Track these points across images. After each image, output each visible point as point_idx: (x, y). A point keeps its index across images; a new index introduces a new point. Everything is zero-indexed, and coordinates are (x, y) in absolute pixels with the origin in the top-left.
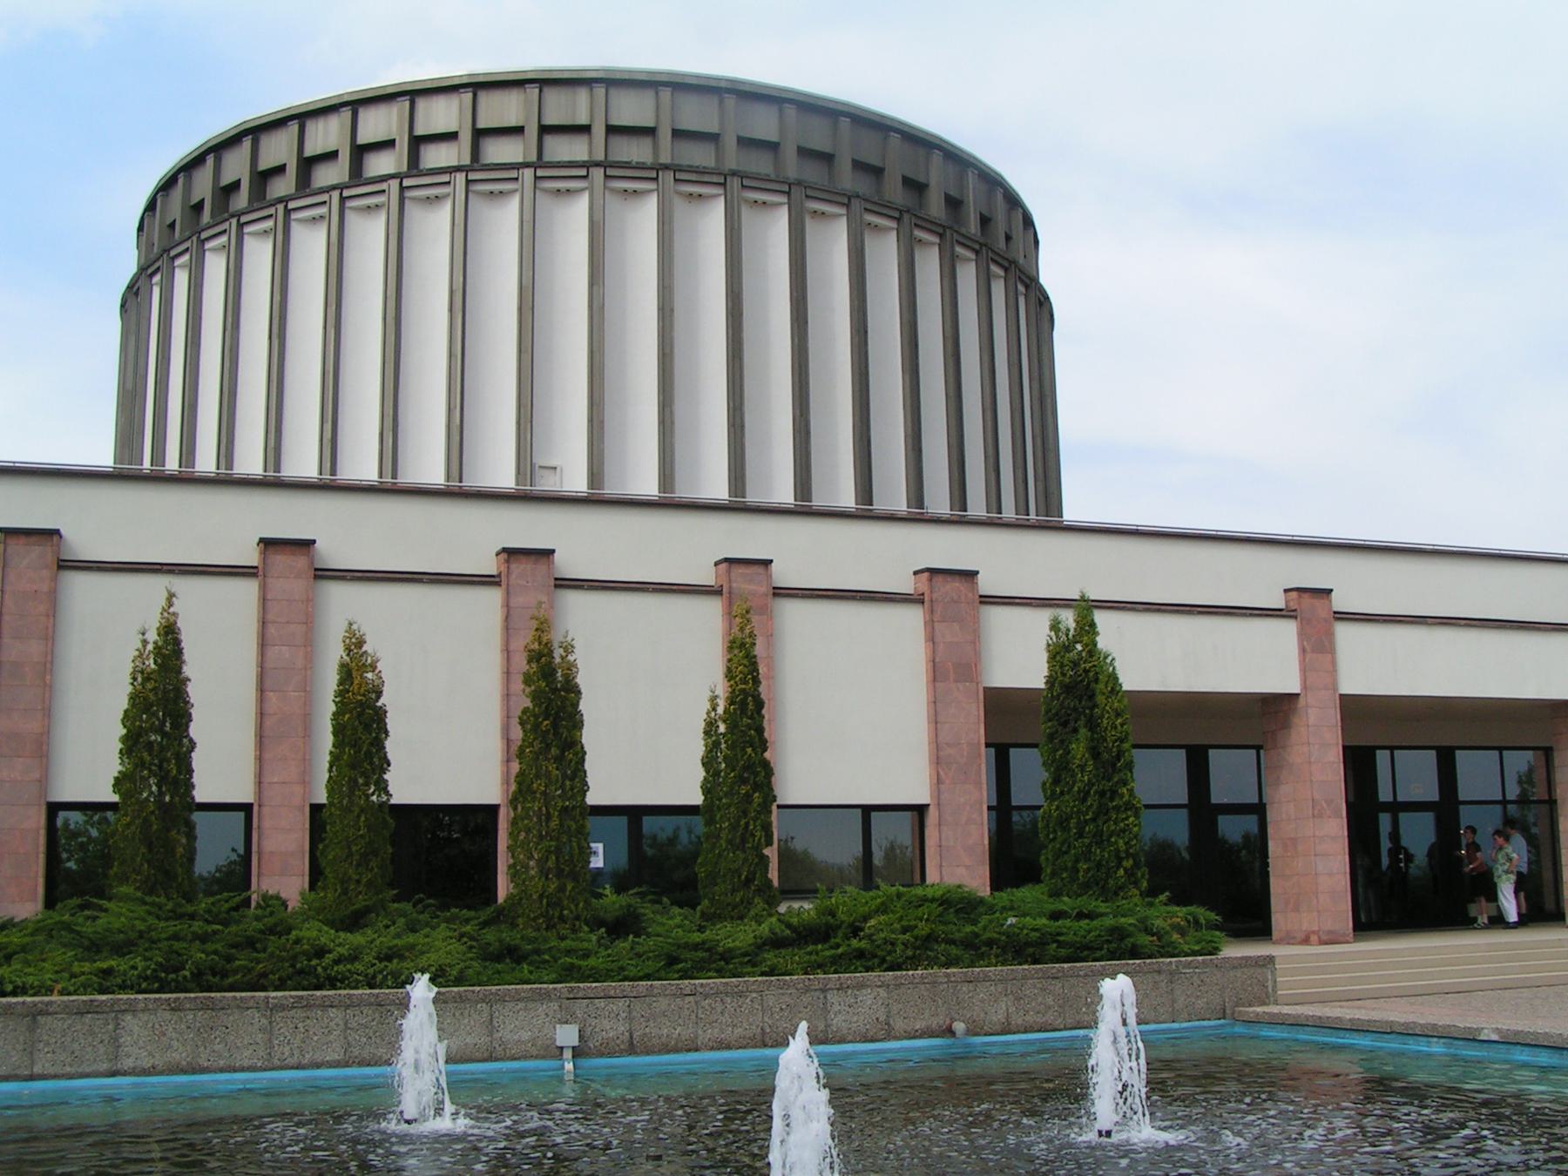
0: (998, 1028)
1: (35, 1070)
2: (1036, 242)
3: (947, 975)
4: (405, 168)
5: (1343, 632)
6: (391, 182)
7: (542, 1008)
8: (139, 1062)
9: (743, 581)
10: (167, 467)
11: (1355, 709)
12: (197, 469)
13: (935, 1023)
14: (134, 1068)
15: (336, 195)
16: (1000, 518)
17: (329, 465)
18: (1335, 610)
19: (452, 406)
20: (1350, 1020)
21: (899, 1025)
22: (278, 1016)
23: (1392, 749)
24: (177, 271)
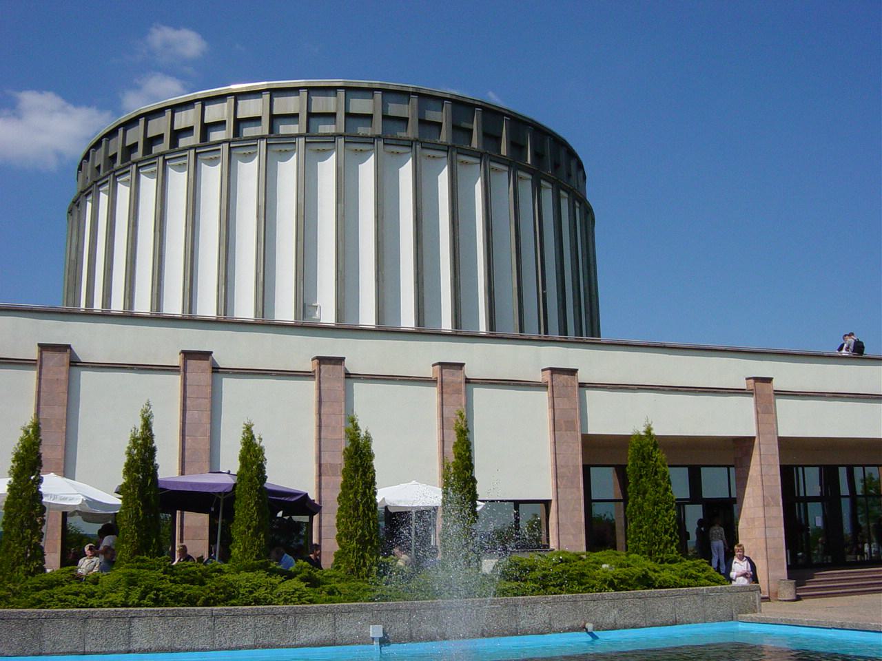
0: (610, 626)
1: (86, 649)
2: (585, 178)
3: (582, 597)
4: (231, 136)
5: (781, 403)
6: (224, 145)
7: (363, 616)
8: (142, 646)
9: (449, 375)
10: (95, 308)
11: (787, 445)
12: (112, 309)
13: (575, 623)
14: (140, 649)
15: (192, 151)
16: (582, 339)
17: (188, 304)
18: (775, 389)
19: (258, 271)
20: (807, 621)
21: (556, 625)
22: (218, 621)
23: (803, 466)
24: (101, 194)
